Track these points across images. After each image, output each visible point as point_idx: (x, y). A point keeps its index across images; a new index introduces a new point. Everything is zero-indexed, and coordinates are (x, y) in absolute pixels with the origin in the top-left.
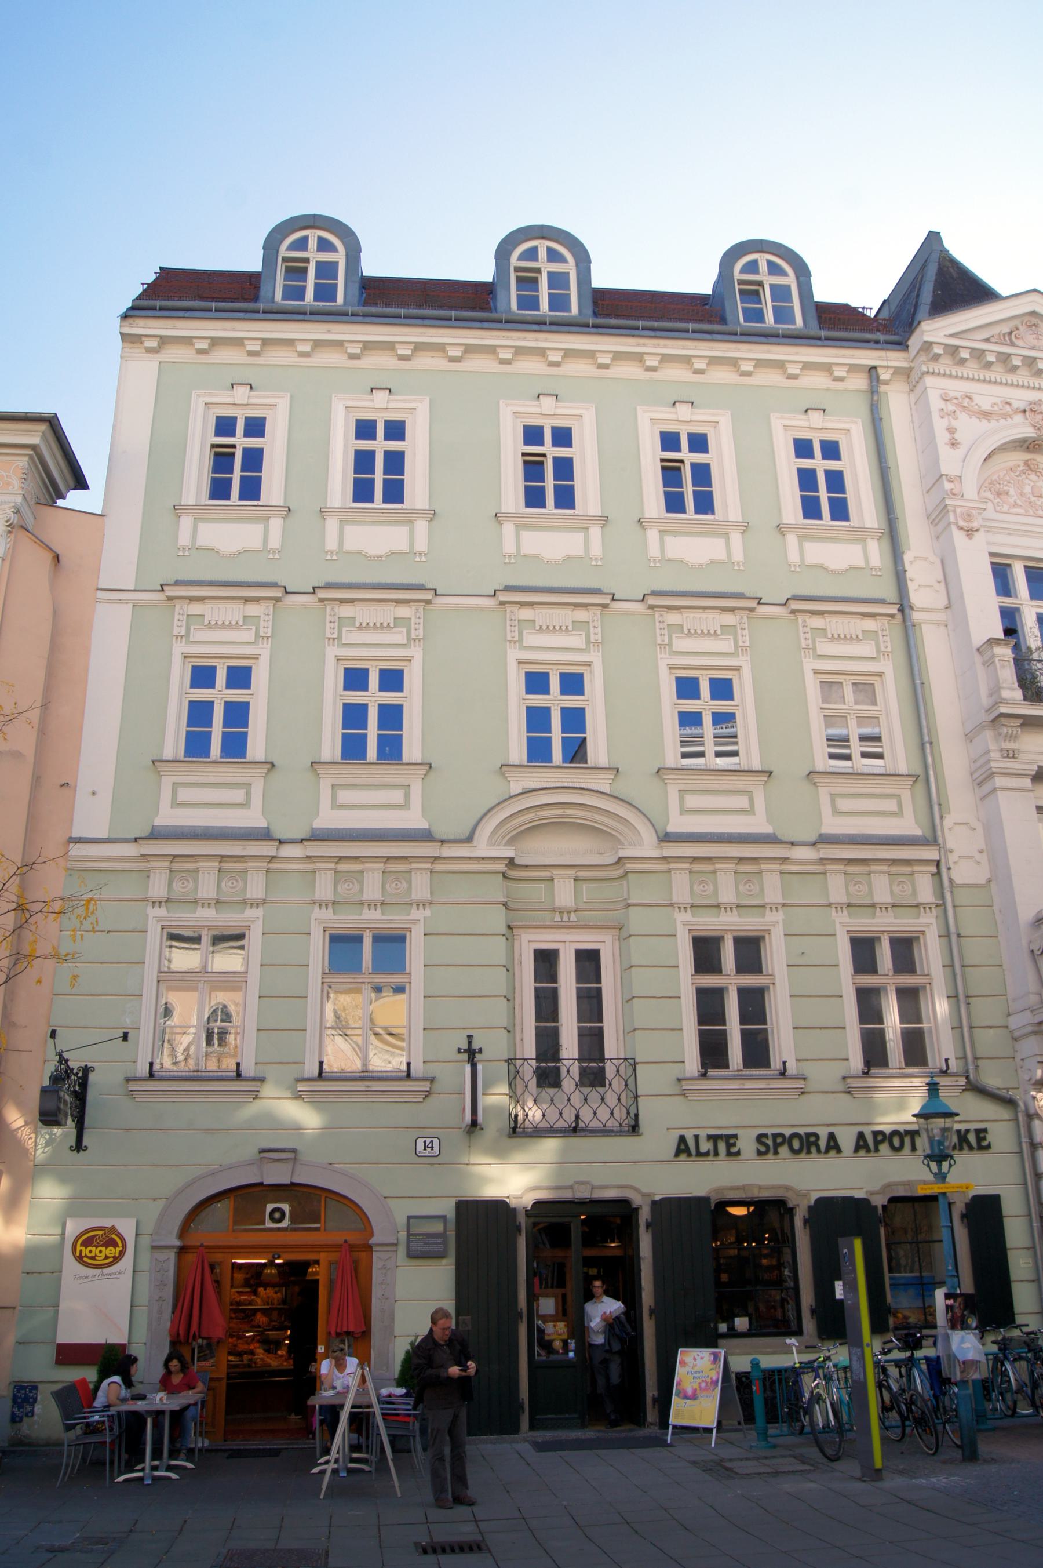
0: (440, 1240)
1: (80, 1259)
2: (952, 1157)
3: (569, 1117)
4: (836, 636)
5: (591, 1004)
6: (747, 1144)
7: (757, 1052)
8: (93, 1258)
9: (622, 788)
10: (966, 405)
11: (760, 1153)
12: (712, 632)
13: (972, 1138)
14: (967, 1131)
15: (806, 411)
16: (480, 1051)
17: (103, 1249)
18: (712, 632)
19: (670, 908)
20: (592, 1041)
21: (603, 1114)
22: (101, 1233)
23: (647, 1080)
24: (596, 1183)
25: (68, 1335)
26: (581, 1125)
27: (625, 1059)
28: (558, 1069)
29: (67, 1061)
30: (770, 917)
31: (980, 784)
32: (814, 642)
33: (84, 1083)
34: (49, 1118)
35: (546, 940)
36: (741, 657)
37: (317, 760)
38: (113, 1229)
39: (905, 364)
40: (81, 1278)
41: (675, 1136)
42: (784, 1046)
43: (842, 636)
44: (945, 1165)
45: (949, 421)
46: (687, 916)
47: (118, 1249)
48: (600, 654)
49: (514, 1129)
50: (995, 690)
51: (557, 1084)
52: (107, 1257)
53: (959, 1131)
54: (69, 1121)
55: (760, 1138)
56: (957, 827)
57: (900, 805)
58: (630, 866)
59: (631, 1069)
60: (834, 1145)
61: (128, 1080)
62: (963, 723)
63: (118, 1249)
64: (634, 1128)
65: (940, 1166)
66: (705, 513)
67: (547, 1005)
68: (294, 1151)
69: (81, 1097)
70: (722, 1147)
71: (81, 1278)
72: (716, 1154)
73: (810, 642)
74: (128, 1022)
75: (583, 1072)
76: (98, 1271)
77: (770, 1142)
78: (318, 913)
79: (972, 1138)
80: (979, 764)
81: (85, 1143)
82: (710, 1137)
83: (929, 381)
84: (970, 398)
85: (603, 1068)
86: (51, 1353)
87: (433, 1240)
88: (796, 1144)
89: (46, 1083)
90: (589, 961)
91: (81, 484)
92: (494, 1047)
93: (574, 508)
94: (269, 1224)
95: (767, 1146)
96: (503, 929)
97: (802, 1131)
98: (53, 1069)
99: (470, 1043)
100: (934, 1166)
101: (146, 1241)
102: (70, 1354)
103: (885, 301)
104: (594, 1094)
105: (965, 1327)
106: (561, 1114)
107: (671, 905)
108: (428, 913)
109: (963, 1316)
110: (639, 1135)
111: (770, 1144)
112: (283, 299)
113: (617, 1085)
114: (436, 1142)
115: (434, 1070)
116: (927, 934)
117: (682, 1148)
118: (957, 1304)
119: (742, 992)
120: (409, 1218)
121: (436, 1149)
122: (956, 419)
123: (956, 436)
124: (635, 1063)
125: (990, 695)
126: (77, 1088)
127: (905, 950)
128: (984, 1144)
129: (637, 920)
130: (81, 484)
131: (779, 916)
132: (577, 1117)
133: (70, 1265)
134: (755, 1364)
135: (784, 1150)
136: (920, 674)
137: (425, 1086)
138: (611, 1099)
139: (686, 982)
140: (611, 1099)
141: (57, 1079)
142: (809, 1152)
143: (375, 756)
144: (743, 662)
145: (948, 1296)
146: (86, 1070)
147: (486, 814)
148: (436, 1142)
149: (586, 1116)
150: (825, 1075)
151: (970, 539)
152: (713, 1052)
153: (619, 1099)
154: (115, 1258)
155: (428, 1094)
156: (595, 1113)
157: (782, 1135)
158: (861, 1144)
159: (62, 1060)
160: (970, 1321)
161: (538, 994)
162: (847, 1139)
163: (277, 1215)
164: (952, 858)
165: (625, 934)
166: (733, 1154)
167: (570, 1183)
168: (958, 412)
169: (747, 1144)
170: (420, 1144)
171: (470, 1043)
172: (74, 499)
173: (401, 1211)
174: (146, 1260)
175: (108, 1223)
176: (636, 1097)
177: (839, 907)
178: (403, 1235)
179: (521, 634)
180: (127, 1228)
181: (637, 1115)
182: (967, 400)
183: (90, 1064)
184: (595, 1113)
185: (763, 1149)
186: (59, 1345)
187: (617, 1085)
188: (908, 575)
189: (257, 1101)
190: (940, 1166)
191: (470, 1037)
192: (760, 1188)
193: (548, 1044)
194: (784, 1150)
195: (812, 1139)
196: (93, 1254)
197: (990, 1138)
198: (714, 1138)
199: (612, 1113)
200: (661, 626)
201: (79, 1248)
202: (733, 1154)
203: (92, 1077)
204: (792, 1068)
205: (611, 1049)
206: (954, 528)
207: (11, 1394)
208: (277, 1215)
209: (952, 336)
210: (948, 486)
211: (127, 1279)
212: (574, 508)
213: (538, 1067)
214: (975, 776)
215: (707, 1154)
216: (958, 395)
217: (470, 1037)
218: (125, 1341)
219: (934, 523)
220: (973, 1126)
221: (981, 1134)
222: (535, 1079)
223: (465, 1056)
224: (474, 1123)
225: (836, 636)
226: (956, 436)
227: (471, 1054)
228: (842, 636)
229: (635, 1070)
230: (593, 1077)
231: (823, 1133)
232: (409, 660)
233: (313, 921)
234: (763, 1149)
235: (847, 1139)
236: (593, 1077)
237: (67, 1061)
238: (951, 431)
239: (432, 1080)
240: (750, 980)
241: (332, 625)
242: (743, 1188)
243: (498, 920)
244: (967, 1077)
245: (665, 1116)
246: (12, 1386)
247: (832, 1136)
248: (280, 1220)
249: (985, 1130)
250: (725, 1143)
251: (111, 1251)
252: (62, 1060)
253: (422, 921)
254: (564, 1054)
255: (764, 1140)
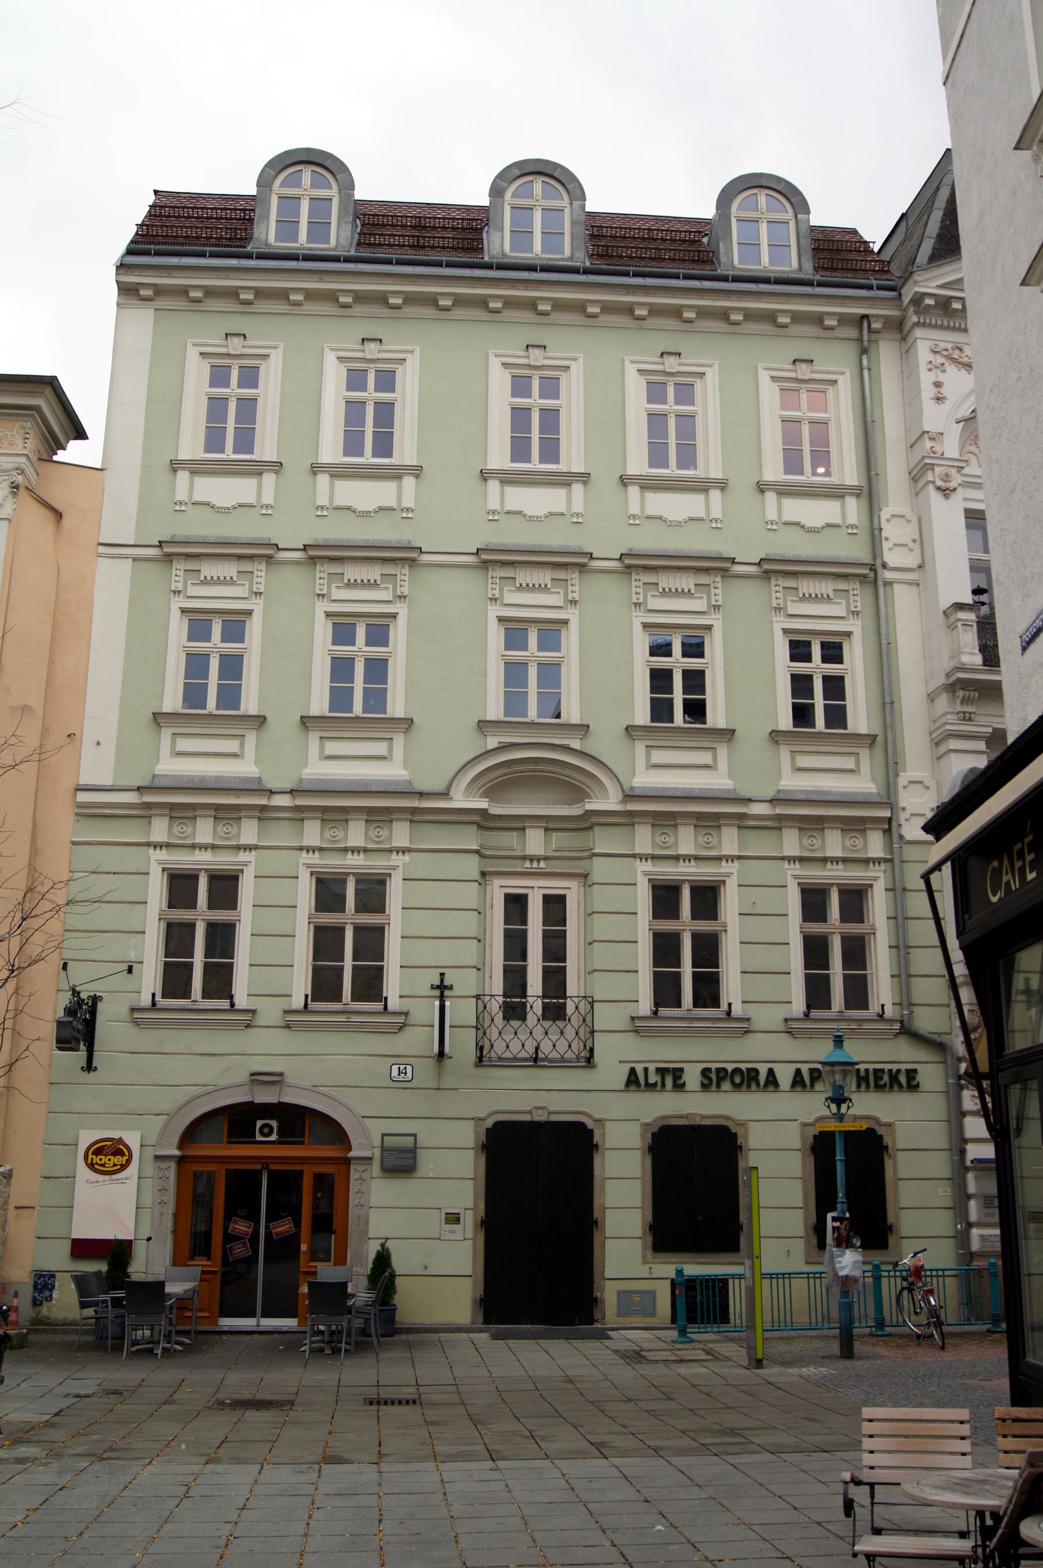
0: (410, 1155)
1: (91, 1166)
2: (851, 1100)
3: (530, 1048)
4: (807, 595)
5: (555, 948)
6: (692, 1077)
7: (708, 990)
8: (103, 1165)
9: (592, 746)
10: (955, 356)
11: (703, 1085)
12: (686, 591)
13: (903, 1079)
14: (899, 1071)
15: (794, 361)
16: (451, 988)
17: (112, 1158)
18: (686, 591)
19: (632, 859)
20: (555, 980)
21: (562, 1046)
22: (109, 1143)
23: (605, 1017)
24: (551, 1109)
25: (83, 1231)
26: (541, 1055)
27: (585, 997)
28: (524, 1004)
29: (79, 993)
30: (725, 867)
31: (937, 744)
32: (785, 601)
33: (93, 1011)
34: (64, 1043)
35: (516, 885)
36: (714, 616)
37: (306, 715)
38: (120, 1140)
39: (896, 313)
40: (92, 1183)
41: (627, 1068)
42: (733, 988)
43: (813, 596)
44: (844, 1107)
45: (937, 376)
46: (648, 866)
47: (125, 1158)
48: (577, 612)
49: (480, 1059)
50: (956, 654)
51: (523, 1018)
52: (115, 1165)
53: (890, 1071)
54: (82, 1047)
55: (705, 1072)
56: (912, 786)
57: (858, 763)
58: (595, 820)
59: (589, 1007)
60: (772, 1080)
61: (133, 1010)
62: (926, 683)
63: (125, 1158)
64: (589, 1061)
65: (839, 1107)
66: (688, 469)
67: (515, 945)
68: (281, 1074)
69: (90, 1026)
70: (669, 1081)
71: (92, 1183)
72: (663, 1085)
73: (781, 601)
74: (132, 956)
75: (545, 1007)
76: (107, 1177)
77: (713, 1076)
78: (305, 857)
79: (903, 1079)
80: (938, 723)
81: (94, 1064)
82: (659, 1070)
83: (919, 332)
84: (961, 350)
85: (565, 1004)
86: (67, 1246)
87: (404, 1155)
88: (737, 1080)
89: (61, 1013)
90: (555, 905)
91: (80, 434)
92: (463, 983)
93: (558, 463)
94: (259, 1138)
95: (710, 1080)
96: (476, 875)
97: (743, 1066)
98: (68, 1002)
99: (442, 980)
100: (833, 1107)
101: (150, 1152)
102: (82, 1249)
103: (903, 215)
104: (554, 1028)
105: (849, 1245)
106: (523, 1045)
107: (634, 856)
108: (407, 858)
109: (848, 1236)
110: (594, 1067)
111: (714, 1079)
112: (276, 241)
113: (575, 1020)
114: (409, 1068)
115: (408, 1004)
116: (875, 887)
117: (632, 1080)
118: (843, 1226)
119: (696, 937)
120: (383, 1135)
121: (409, 1075)
122: (944, 371)
123: (942, 390)
124: (593, 1001)
125: (952, 658)
126: (88, 1016)
127: (855, 901)
128: (915, 1083)
129: (600, 869)
130: (80, 434)
131: (733, 867)
132: (537, 1049)
133: (83, 1172)
134: (679, 1272)
135: (726, 1085)
136: (887, 635)
137: (401, 1019)
138: (570, 1033)
139: (643, 927)
140: (570, 1033)
141: (70, 1011)
142: (749, 1086)
143: (361, 710)
144: (714, 620)
145: (834, 1219)
146: (95, 1000)
147: (463, 768)
148: (409, 1068)
149: (546, 1048)
150: (767, 1017)
151: (947, 498)
152: (666, 991)
153: (577, 1034)
154: (122, 1165)
155: (402, 1027)
156: (554, 1046)
157: (725, 1070)
158: (798, 1081)
159: (75, 992)
160: (854, 1241)
161: (508, 935)
162: (785, 1075)
163: (266, 1130)
164: (903, 816)
165: (590, 883)
166: (679, 1086)
167: (528, 1108)
168: (947, 364)
169: (692, 1077)
170: (395, 1068)
171: (442, 980)
172: (73, 452)
173: (376, 1129)
174: (150, 1169)
175: (116, 1135)
176: (592, 1032)
177: (791, 859)
178: (377, 1153)
179: (501, 591)
180: (132, 1139)
181: (592, 1050)
182: (957, 352)
183: (98, 994)
184: (554, 1046)
185: (706, 1082)
186: (73, 1240)
187: (575, 1020)
188: (884, 534)
189: (249, 1030)
190: (839, 1107)
191: (442, 974)
192: (703, 1117)
193: (515, 978)
194: (726, 1085)
195: (753, 1074)
196: (103, 1162)
197: (920, 1078)
198: (662, 1072)
199: (570, 1046)
200: (637, 583)
201: (90, 1156)
202: (679, 1086)
203: (100, 1006)
204: (737, 1010)
205: (573, 987)
206: (931, 487)
207: (32, 1283)
208: (267, 1130)
209: (943, 286)
210: (929, 444)
211: (132, 1185)
212: (558, 463)
213: (504, 1002)
214: (934, 736)
215: (655, 1085)
216: (949, 346)
217: (442, 974)
218: (131, 1237)
219: (915, 480)
220: (903, 1067)
221: (911, 1074)
222: (501, 1014)
223: (437, 993)
224: (441, 1054)
225: (807, 595)
226: (942, 390)
227: (442, 988)
228: (813, 596)
229: (592, 1007)
230: (555, 1012)
231: (763, 1070)
232: (394, 616)
233: (301, 866)
234: (706, 1082)
235: (785, 1075)
236: (555, 1012)
237: (79, 993)
238: (938, 385)
239: (406, 1014)
240: (704, 926)
241: (322, 581)
242: (686, 1116)
243: (471, 866)
244: (902, 1022)
245: (616, 1053)
246: (33, 1275)
247: (771, 1072)
248: (269, 1134)
249: (915, 1071)
250: (672, 1077)
251: (119, 1160)
252: (75, 992)
253: (401, 868)
254: (530, 991)
255: (708, 1074)
